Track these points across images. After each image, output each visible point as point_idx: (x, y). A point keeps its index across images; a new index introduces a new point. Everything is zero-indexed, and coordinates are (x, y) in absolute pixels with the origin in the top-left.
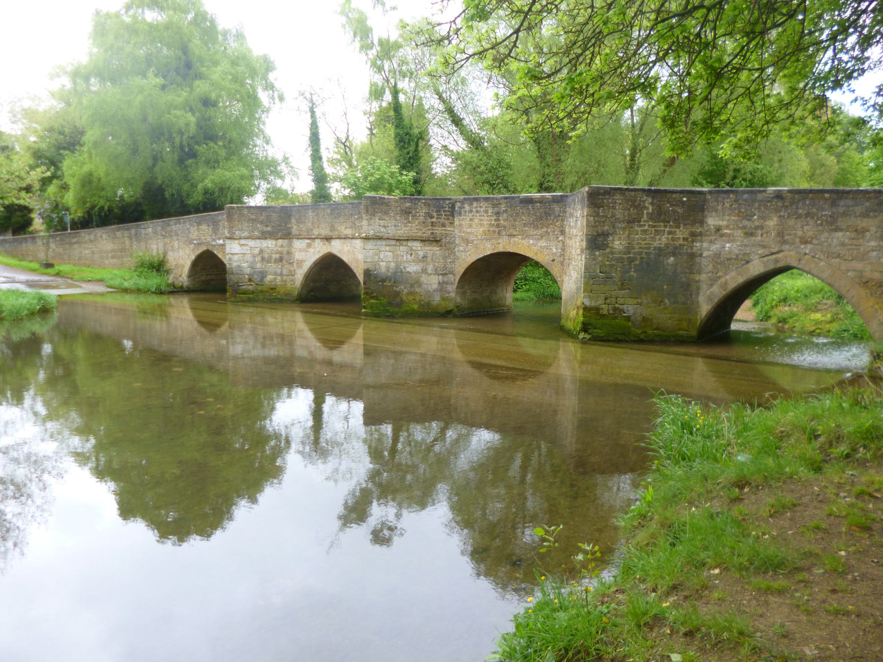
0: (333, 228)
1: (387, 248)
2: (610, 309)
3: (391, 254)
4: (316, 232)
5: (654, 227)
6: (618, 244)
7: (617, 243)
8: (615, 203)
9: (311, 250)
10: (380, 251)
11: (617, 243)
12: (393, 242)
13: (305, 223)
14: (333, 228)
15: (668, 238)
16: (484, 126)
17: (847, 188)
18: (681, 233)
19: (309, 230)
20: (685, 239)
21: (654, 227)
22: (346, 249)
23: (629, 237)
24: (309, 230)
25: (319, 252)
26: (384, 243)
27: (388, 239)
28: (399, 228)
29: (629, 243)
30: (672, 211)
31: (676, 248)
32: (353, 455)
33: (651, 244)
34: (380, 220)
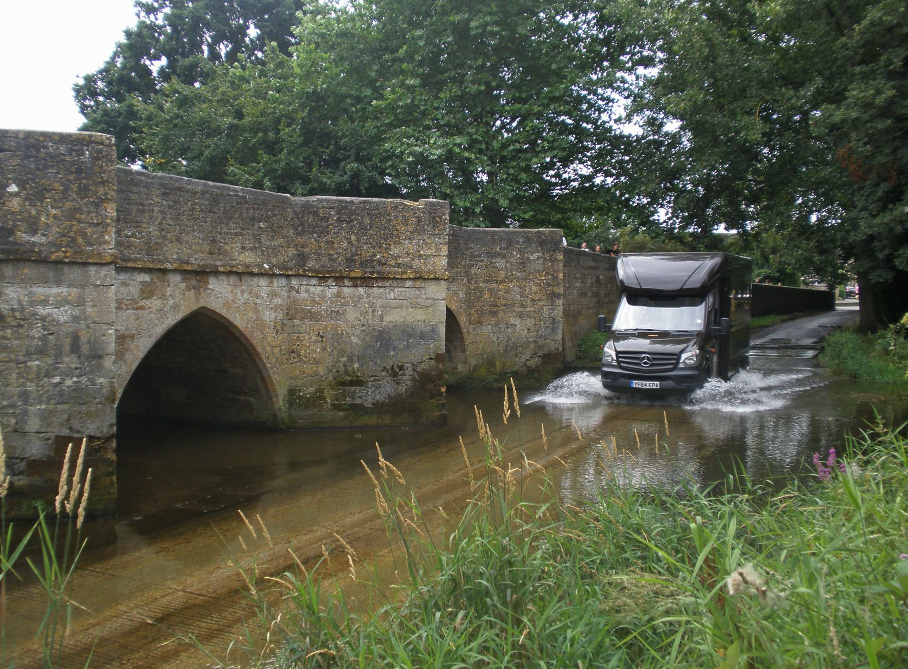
0: (216, 250)
4: (172, 253)
9: (155, 303)
13: (138, 224)
14: (216, 250)
16: (364, 113)
17: (442, 330)
19: (150, 248)
22: (242, 298)
24: (150, 248)
25: (176, 308)
32: (325, 260)
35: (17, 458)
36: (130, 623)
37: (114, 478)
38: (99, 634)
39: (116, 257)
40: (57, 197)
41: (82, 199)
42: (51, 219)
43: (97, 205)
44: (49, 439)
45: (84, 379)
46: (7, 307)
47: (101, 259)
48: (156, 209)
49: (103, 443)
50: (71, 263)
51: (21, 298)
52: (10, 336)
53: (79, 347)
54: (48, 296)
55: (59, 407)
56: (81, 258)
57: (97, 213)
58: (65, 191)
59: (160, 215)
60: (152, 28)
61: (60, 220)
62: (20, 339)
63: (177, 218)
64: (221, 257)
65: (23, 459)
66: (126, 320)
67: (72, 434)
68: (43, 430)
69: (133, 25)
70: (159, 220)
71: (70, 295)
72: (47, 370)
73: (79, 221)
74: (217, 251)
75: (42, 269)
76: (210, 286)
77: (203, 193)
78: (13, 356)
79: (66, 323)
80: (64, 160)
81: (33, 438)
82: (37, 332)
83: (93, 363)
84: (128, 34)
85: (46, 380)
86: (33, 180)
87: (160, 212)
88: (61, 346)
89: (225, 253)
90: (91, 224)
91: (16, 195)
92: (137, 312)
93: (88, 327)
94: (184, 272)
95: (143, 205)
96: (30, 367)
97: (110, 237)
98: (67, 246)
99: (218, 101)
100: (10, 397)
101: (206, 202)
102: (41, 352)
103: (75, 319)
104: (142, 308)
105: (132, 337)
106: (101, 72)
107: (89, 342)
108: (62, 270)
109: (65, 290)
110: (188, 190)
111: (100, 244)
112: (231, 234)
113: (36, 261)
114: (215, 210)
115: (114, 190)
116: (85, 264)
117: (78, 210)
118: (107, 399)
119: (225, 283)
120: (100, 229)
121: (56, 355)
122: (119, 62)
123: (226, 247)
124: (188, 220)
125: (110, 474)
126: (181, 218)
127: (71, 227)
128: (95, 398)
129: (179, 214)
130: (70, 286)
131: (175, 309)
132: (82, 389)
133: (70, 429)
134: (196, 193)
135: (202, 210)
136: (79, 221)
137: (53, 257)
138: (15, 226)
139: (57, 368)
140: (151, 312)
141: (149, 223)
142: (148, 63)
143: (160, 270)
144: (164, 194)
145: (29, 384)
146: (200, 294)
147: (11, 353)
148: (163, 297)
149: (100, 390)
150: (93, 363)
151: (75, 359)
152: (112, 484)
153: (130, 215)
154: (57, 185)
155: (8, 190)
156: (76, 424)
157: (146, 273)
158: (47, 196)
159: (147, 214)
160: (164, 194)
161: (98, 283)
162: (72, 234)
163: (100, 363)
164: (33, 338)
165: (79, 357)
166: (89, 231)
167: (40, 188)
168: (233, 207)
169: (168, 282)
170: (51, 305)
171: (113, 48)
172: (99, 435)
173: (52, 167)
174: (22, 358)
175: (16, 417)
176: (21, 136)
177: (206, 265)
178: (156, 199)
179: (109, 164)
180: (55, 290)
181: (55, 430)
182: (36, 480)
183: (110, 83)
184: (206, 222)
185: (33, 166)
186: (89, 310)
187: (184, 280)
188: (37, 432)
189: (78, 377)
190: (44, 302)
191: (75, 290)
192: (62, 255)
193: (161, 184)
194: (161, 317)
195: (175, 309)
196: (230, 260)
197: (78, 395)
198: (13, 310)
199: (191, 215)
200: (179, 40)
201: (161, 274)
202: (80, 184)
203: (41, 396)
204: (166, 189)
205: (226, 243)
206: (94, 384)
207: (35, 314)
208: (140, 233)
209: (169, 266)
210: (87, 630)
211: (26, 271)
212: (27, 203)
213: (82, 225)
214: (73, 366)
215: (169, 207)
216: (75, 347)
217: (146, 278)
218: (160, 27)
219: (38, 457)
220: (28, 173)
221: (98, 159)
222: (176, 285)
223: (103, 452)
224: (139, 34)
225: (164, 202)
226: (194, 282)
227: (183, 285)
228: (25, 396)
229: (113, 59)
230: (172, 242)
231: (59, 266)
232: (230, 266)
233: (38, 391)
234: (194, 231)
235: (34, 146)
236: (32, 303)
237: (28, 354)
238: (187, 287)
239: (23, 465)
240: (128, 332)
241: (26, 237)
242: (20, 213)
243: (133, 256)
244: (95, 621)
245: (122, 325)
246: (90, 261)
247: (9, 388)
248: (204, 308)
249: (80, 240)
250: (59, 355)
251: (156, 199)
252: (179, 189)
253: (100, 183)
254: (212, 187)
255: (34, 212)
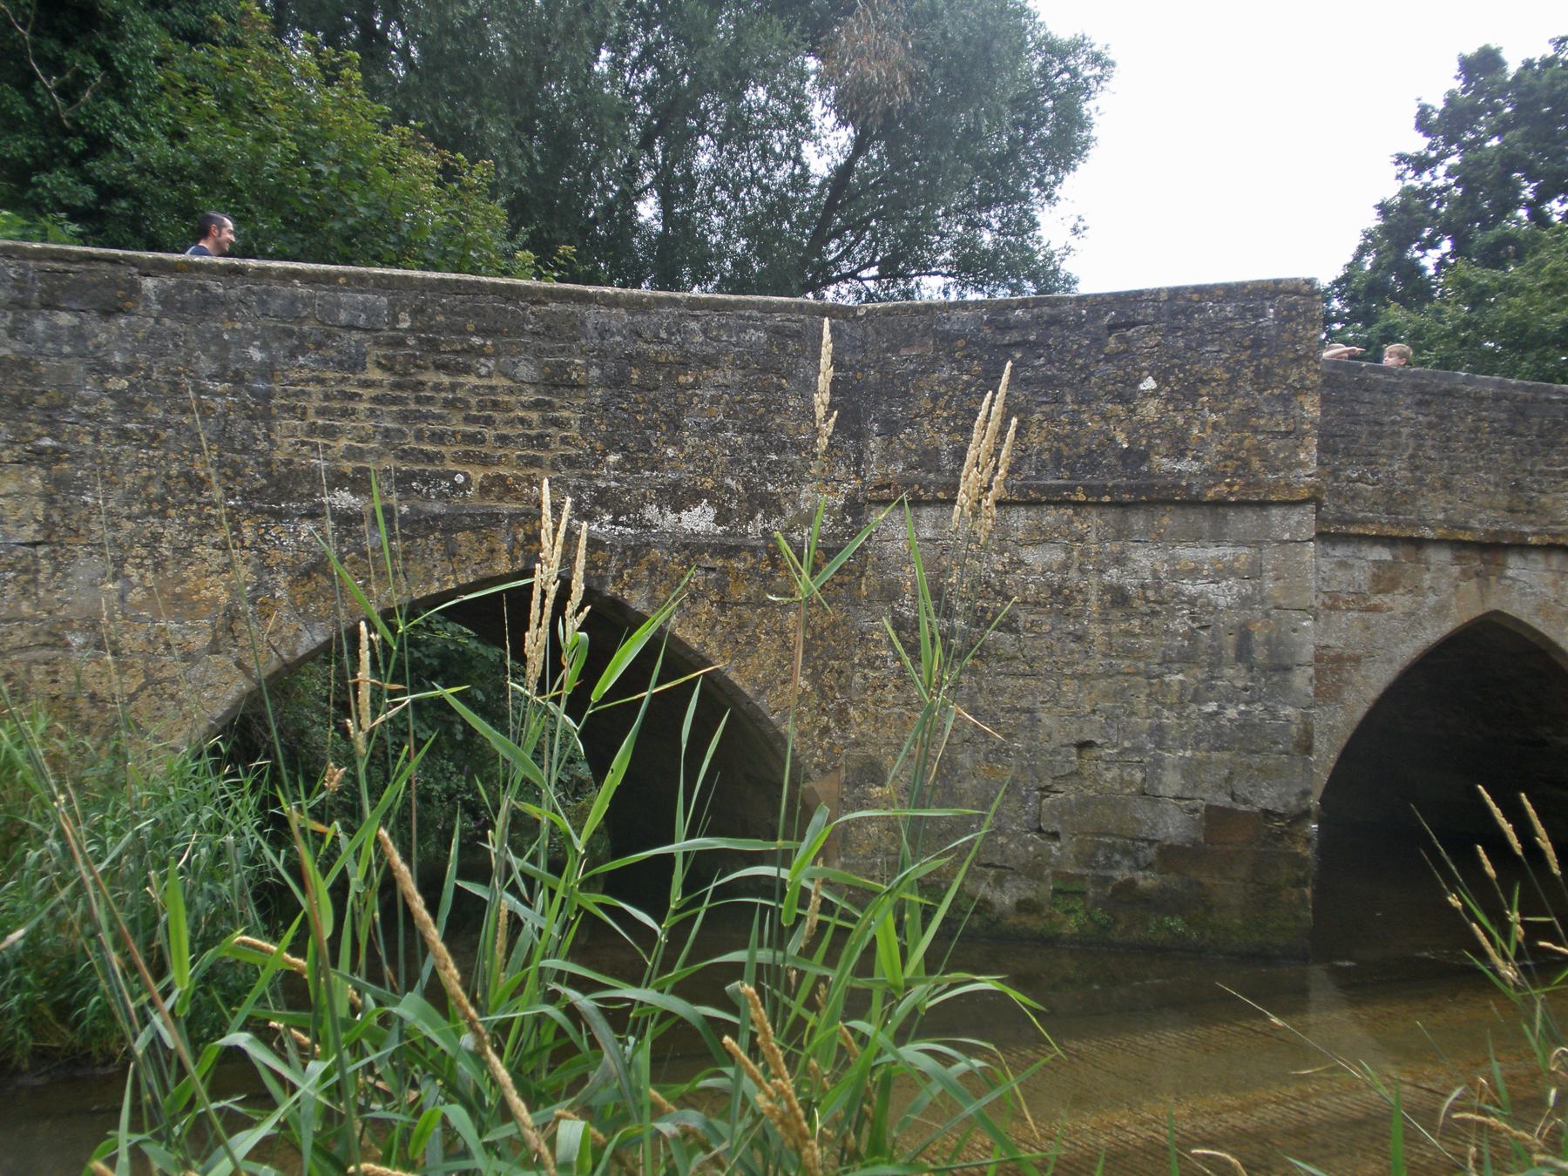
4: (1434, 511)
9: (1399, 601)
13: (1370, 459)
14: (1520, 500)
24: (1393, 501)
25: (1440, 611)
35: (1143, 840)
36: (1300, 1117)
37: (1308, 892)
38: (1239, 1123)
39: (1318, 489)
40: (1219, 391)
41: (1261, 391)
42: (1209, 431)
43: (1285, 400)
44: (1196, 810)
45: (1258, 708)
46: (1135, 582)
47: (1291, 493)
48: (1405, 431)
49: (1289, 825)
50: (1240, 504)
51: (1158, 566)
52: (1137, 630)
53: (1250, 652)
54: (1202, 562)
55: (1215, 755)
56: (1258, 494)
57: (1287, 413)
58: (1233, 380)
59: (1412, 442)
60: (1426, 193)
61: (1224, 431)
62: (1153, 635)
63: (1444, 446)
64: (1532, 517)
65: (1151, 842)
66: (1344, 631)
67: (1234, 805)
68: (1188, 794)
69: (1390, 190)
70: (1410, 451)
71: (1236, 559)
72: (1196, 690)
73: (1255, 431)
74: (1523, 507)
75: (1192, 516)
76: (1510, 573)
77: (1497, 398)
78: (1141, 665)
79: (1229, 608)
80: (1232, 328)
81: (1170, 806)
82: (1180, 624)
83: (1275, 679)
84: (1384, 209)
85: (1193, 707)
86: (1181, 367)
87: (1412, 435)
88: (1221, 648)
89: (1543, 511)
90: (1275, 435)
91: (1154, 394)
92: (1366, 615)
93: (1267, 615)
94: (1458, 546)
95: (1381, 424)
96: (1168, 685)
97: (1309, 454)
98: (1235, 474)
99: (1544, 288)
100: (1135, 735)
101: (1503, 416)
102: (1187, 658)
103: (1245, 601)
104: (1375, 609)
105: (1357, 660)
106: (1337, 283)
107: (1268, 642)
108: (1225, 516)
109: (1230, 551)
110: (1468, 395)
111: (1290, 468)
112: (1554, 474)
113: (1182, 504)
114: (1521, 429)
115: (1316, 371)
116: (1264, 504)
117: (1250, 411)
118: (1297, 745)
119: (1541, 566)
120: (1290, 441)
121: (1210, 665)
122: (1368, 261)
123: (1543, 499)
124: (1467, 449)
125: (1300, 883)
126: (1453, 445)
127: (1241, 441)
128: (1276, 743)
129: (1449, 439)
130: (1238, 544)
131: (1438, 612)
132: (1254, 725)
133: (1233, 796)
134: (1483, 399)
135: (1494, 431)
136: (1255, 431)
137: (1211, 494)
138: (1150, 446)
139: (1213, 687)
140: (1392, 617)
141: (1391, 457)
142: (1418, 254)
143: (1410, 541)
144: (1420, 403)
145: (1166, 713)
146: (1488, 586)
147: (1139, 659)
148: (1416, 590)
149: (1284, 729)
150: (1275, 679)
151: (1243, 672)
152: (1303, 899)
153: (1356, 442)
154: (1219, 373)
155: (1142, 387)
156: (1242, 788)
157: (1384, 545)
158: (1203, 392)
159: (1386, 441)
160: (1420, 403)
161: (1287, 536)
162: (1243, 454)
163: (1286, 680)
164: (1175, 634)
165: (1250, 669)
166: (1272, 446)
167: (1192, 380)
168: (1557, 423)
169: (1427, 562)
170: (1206, 577)
171: (1356, 241)
172: (1281, 810)
173: (1212, 341)
174: (1155, 669)
175: (1143, 770)
176: (1164, 296)
177: (1502, 533)
178: (1406, 413)
179: (1309, 326)
180: (1213, 552)
181: (1205, 796)
182: (1173, 880)
183: (1352, 300)
184: (1502, 452)
185: (1181, 344)
186: (1269, 585)
187: (1458, 559)
188: (1176, 798)
189: (1247, 703)
190: (1194, 573)
191: (1246, 550)
192: (1225, 489)
193: (1415, 386)
194: (1412, 626)
195: (1438, 612)
196: (1552, 523)
197: (1247, 736)
198: (1143, 586)
199: (1472, 440)
200: (1474, 205)
201: (1412, 549)
202: (1257, 367)
203: (1184, 734)
204: (1424, 393)
205: (1542, 492)
206: (1275, 717)
207: (1180, 593)
208: (1373, 474)
209: (1428, 533)
210: (1217, 1113)
211: (1166, 521)
212: (1170, 407)
213: (1260, 437)
214: (1240, 684)
215: (1430, 426)
216: (1244, 651)
217: (1383, 554)
218: (1439, 191)
219: (1177, 841)
220: (1173, 357)
221: (1290, 319)
222: (1441, 570)
223: (1288, 842)
224: (1404, 208)
225: (1421, 418)
226: (1477, 564)
227: (1455, 570)
228: (1158, 732)
229: (1358, 258)
230: (1434, 490)
231: (1220, 510)
232: (1553, 535)
233: (1181, 726)
234: (1478, 469)
235: (1183, 311)
236: (1174, 575)
237: (1166, 661)
238: (1464, 572)
239: (1152, 853)
240: (1348, 652)
241: (1167, 464)
242: (1159, 423)
243: (1360, 515)
244: (1236, 1103)
245: (1338, 638)
246: (1273, 498)
247: (1134, 719)
248: (1497, 613)
249: (1256, 464)
250: (1216, 663)
251: (1406, 413)
252: (1448, 393)
253: (1293, 360)
254: (1515, 387)
255: (1180, 421)
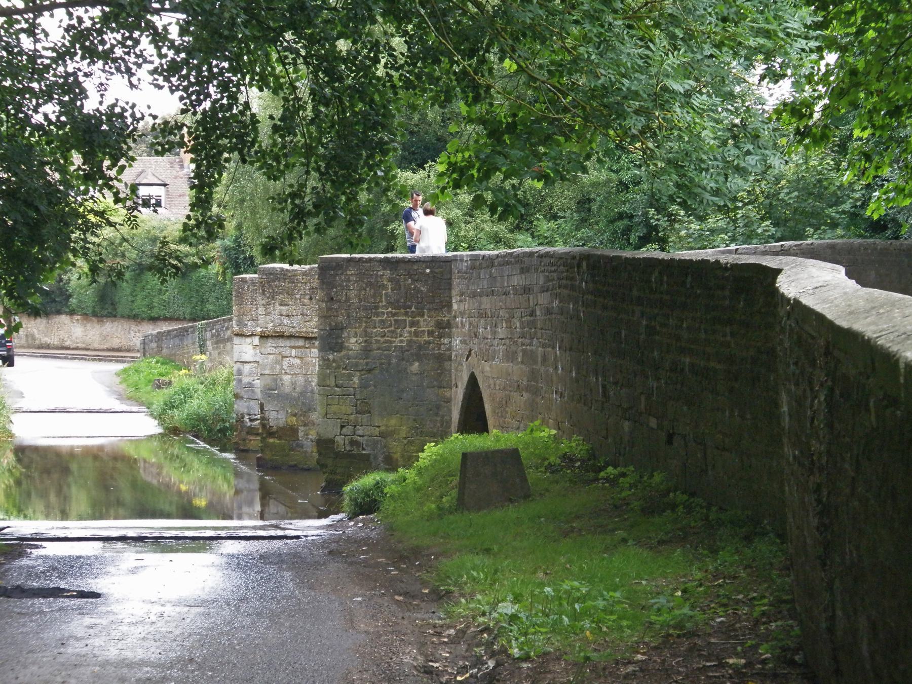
1: (294, 352)
2: (347, 442)
3: (298, 361)
5: (394, 315)
6: (354, 343)
7: (353, 340)
8: (349, 281)
10: (283, 357)
11: (353, 340)
12: (301, 343)
15: (410, 332)
18: (426, 323)
20: (430, 333)
21: (394, 315)
23: (365, 331)
26: (288, 343)
27: (291, 337)
28: (308, 318)
29: (366, 341)
30: (414, 289)
31: (420, 347)
33: (391, 342)
34: (281, 305)
